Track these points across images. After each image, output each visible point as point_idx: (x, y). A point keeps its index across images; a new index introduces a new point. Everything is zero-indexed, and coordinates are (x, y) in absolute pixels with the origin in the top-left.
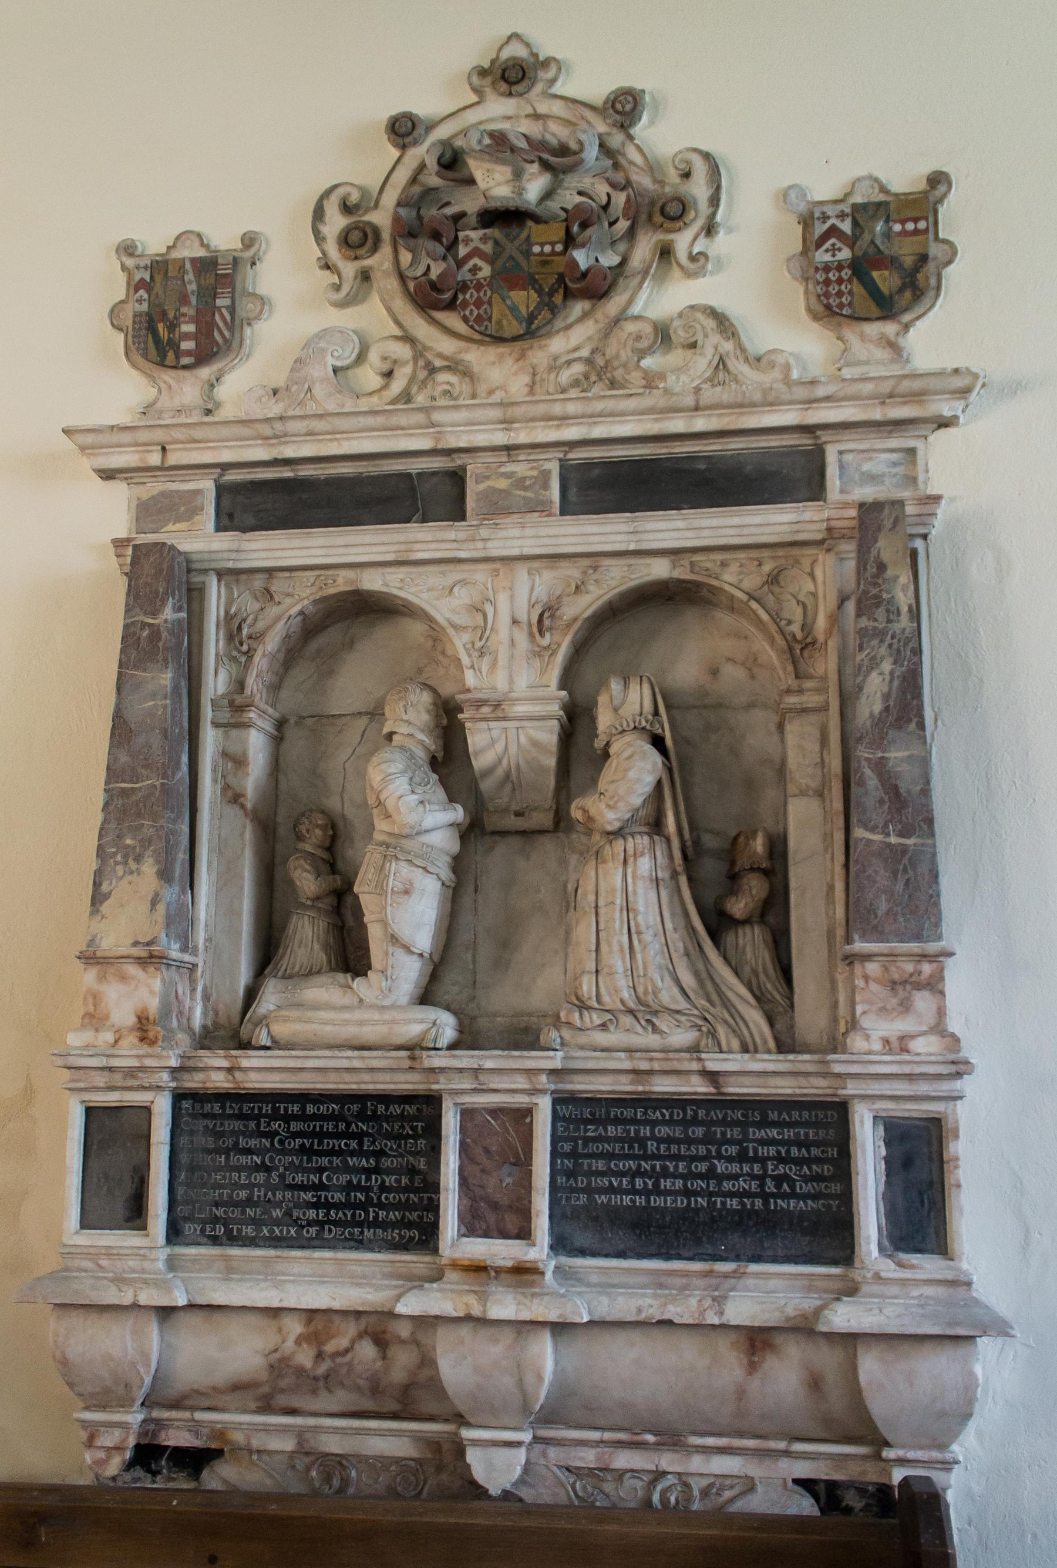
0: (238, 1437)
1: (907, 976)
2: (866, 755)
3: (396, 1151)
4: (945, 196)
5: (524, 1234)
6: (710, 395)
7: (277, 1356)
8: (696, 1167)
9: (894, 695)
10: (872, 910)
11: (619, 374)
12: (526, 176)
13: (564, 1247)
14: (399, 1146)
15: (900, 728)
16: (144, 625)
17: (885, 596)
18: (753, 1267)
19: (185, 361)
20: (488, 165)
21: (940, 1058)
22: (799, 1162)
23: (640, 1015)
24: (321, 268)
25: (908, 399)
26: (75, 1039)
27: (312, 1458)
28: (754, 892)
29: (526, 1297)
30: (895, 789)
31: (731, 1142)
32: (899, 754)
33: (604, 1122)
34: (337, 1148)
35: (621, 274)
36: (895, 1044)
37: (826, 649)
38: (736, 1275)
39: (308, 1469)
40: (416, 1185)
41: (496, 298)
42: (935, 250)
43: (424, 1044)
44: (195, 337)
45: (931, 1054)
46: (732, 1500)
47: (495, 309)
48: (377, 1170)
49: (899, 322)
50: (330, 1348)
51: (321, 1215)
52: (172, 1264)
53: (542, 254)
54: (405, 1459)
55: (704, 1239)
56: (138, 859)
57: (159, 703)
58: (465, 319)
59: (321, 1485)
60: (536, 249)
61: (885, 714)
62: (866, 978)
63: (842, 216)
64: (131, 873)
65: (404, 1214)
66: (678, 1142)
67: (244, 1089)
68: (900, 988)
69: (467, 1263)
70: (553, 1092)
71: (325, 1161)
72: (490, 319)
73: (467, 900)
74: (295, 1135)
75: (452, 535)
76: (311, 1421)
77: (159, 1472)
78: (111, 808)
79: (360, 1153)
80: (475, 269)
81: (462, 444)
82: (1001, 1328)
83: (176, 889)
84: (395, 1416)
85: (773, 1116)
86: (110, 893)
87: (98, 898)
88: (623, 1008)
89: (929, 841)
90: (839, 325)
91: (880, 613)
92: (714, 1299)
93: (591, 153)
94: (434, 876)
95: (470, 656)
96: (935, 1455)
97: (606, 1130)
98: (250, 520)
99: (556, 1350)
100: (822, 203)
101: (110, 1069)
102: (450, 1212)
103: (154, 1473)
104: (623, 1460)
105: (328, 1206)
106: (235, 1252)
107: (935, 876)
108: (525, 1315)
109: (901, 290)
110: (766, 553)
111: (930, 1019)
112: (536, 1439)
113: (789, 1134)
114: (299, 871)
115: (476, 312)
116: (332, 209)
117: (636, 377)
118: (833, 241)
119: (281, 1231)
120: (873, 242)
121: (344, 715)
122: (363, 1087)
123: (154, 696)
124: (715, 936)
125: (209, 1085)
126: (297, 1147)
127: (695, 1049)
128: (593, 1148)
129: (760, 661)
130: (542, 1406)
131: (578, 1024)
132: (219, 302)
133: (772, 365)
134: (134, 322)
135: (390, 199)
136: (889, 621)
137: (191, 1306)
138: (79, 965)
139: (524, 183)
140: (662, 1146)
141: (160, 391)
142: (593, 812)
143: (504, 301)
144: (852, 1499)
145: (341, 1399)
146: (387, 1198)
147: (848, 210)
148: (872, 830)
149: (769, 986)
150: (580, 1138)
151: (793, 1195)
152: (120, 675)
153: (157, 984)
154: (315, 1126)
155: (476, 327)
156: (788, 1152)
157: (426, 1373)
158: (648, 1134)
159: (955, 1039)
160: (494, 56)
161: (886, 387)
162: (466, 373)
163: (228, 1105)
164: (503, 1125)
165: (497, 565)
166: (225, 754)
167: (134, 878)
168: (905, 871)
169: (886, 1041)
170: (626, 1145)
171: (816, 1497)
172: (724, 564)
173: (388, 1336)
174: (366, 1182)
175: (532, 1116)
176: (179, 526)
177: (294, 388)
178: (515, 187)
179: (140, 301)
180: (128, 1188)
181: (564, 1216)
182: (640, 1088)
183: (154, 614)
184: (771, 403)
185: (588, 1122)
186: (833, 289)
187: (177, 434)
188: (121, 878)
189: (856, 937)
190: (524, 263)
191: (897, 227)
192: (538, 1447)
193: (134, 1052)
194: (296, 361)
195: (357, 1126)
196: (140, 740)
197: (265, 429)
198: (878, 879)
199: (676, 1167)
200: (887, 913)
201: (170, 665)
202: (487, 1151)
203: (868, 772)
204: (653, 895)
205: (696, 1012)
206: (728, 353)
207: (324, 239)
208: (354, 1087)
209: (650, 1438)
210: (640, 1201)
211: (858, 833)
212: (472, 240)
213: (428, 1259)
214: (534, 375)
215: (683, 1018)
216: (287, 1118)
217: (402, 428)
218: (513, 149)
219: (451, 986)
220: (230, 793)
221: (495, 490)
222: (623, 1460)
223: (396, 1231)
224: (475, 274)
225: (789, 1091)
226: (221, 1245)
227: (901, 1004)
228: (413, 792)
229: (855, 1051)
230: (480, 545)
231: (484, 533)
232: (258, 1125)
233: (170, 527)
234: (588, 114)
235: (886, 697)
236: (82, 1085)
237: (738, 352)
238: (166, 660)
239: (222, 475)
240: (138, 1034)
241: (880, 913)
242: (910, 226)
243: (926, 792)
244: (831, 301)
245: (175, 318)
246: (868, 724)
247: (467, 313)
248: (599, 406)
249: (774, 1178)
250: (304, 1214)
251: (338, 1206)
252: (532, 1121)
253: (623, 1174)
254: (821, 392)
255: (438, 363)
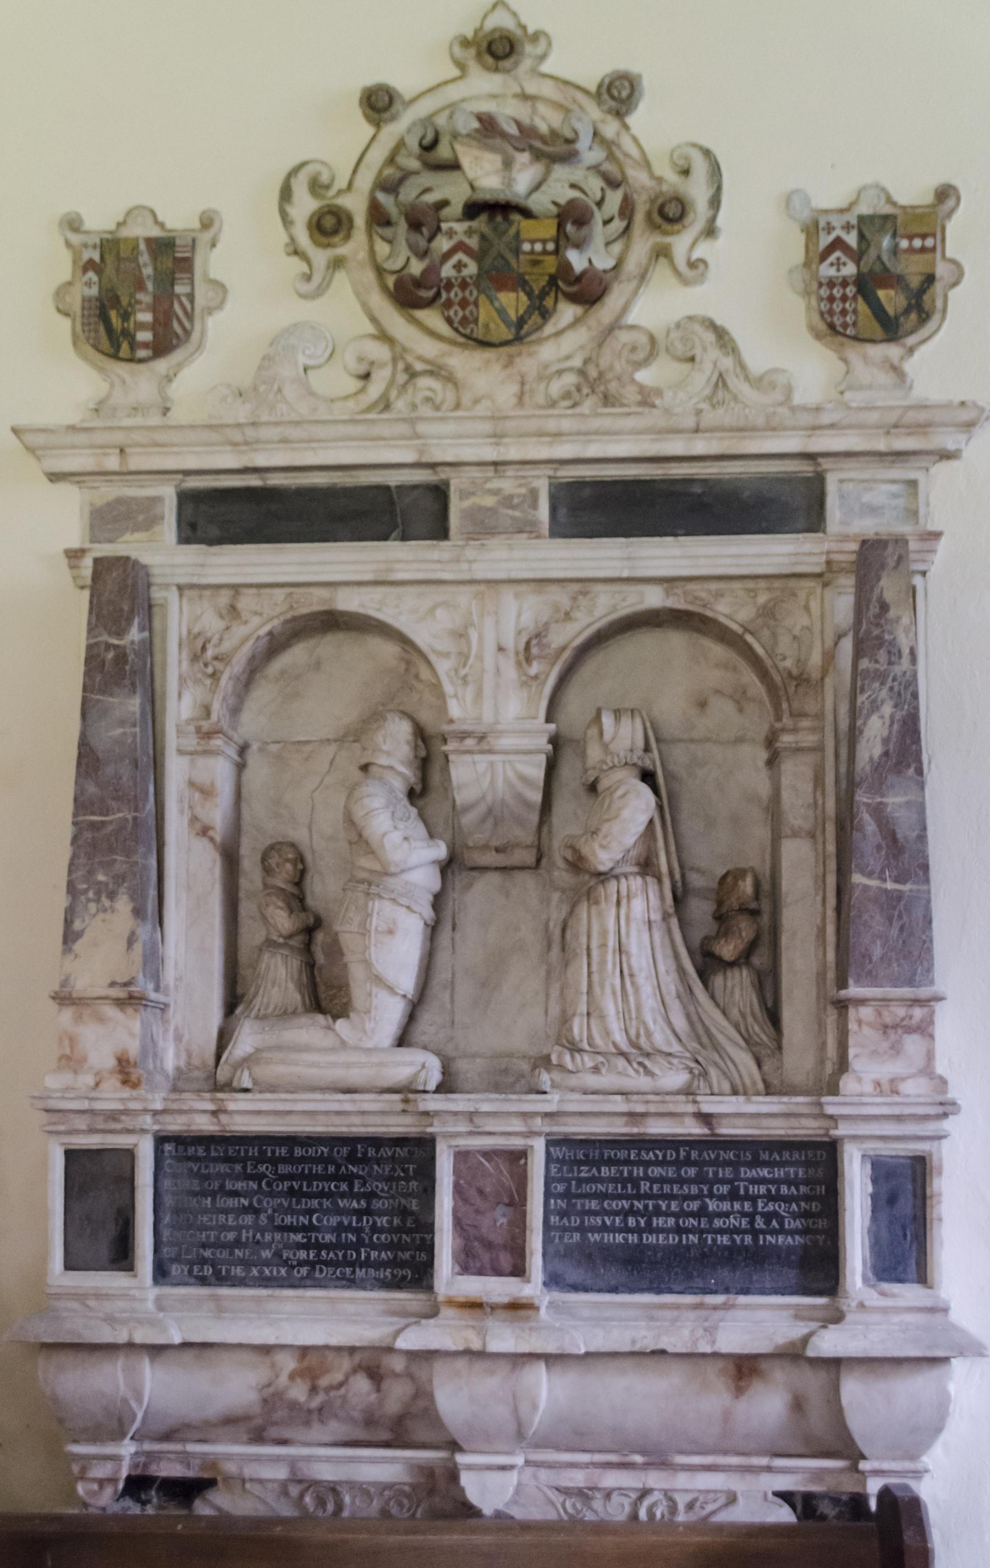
0: (231, 1468)
1: (898, 1020)
2: (865, 800)
3: (388, 1192)
4: (953, 211)
5: (519, 1271)
6: (711, 417)
7: (271, 1390)
8: (688, 1206)
9: (894, 739)
10: (867, 956)
11: (613, 387)
12: (517, 166)
13: (557, 1283)
14: (390, 1188)
15: (899, 772)
16: (108, 646)
17: (887, 637)
18: (742, 1299)
19: (142, 353)
20: (476, 152)
21: (929, 1100)
22: (788, 1200)
23: (632, 1057)
24: (289, 254)
25: (911, 430)
26: (54, 1082)
27: (306, 1485)
28: (744, 934)
29: (523, 1331)
30: (894, 839)
31: (723, 1181)
32: (900, 799)
33: (598, 1163)
34: (326, 1190)
35: (616, 278)
36: (886, 1087)
37: (823, 686)
38: (726, 1307)
39: (302, 1496)
40: (408, 1225)
41: (483, 299)
42: (941, 270)
43: (413, 1087)
44: (153, 327)
45: (919, 1096)
46: (714, 1513)
47: (482, 310)
48: (368, 1212)
49: (904, 346)
50: (324, 1382)
51: (312, 1255)
52: (160, 1305)
53: (532, 252)
54: (400, 1484)
55: (695, 1274)
56: (112, 896)
57: (128, 730)
58: (449, 321)
59: (315, 1510)
60: (526, 247)
61: (884, 759)
62: (860, 1022)
63: (847, 227)
64: (105, 910)
65: (396, 1254)
66: (671, 1181)
67: (231, 1132)
68: (890, 1031)
69: (463, 1300)
70: (547, 1134)
71: (315, 1203)
72: (476, 321)
73: (445, 937)
74: (283, 1178)
75: (436, 555)
76: (305, 1451)
77: (149, 1501)
78: (80, 842)
79: (351, 1195)
80: (459, 266)
81: (449, 458)
82: (972, 1349)
83: (149, 927)
84: (387, 1445)
85: (765, 1156)
86: (83, 931)
87: (70, 937)
88: (614, 1051)
89: (924, 887)
90: (842, 345)
91: (882, 655)
92: (705, 1330)
93: (583, 143)
94: (418, 916)
95: (453, 683)
96: (908, 1465)
97: (599, 1172)
98: (214, 531)
99: (549, 1380)
100: (826, 212)
101: (92, 1112)
102: (445, 1250)
103: (144, 1503)
104: (611, 1479)
105: (319, 1246)
106: (224, 1291)
107: (928, 921)
108: (524, 1348)
109: (907, 311)
110: (762, 584)
111: (920, 1062)
112: (528, 1463)
113: (779, 1173)
114: (271, 908)
115: (461, 314)
116: (300, 188)
117: (631, 394)
118: (838, 254)
119: (271, 1272)
120: (879, 258)
121: (333, 760)
122: (354, 1129)
123: (122, 723)
124: (704, 976)
125: (194, 1128)
126: (285, 1189)
127: (688, 1092)
128: (586, 1188)
129: (749, 694)
130: (534, 1433)
131: (570, 1066)
132: (179, 289)
133: (773, 385)
134: (83, 308)
135: (365, 181)
136: (890, 663)
137: (186, 1345)
138: (53, 1006)
139: (514, 173)
140: (655, 1186)
141: (112, 385)
142: (585, 851)
143: (492, 302)
144: (826, 1508)
145: (335, 1429)
146: (378, 1239)
147: (854, 222)
148: (870, 875)
149: (757, 1028)
150: (573, 1179)
151: (782, 1231)
152: (85, 702)
153: (137, 1026)
154: (303, 1169)
155: (461, 329)
156: (778, 1190)
157: (421, 1403)
158: (641, 1174)
159: (943, 1082)
160: (478, 25)
161: (892, 417)
162: (450, 379)
163: (212, 1148)
164: (497, 1167)
165: (482, 588)
166: (192, 784)
167: (108, 916)
168: (900, 917)
169: (878, 1084)
170: (619, 1186)
171: (793, 1507)
172: (719, 595)
173: (382, 1371)
174: (357, 1223)
175: (526, 1158)
176: (138, 536)
177: (262, 388)
178: (504, 178)
179: (89, 284)
180: (111, 1230)
181: (557, 1253)
182: (635, 1130)
183: (120, 634)
184: (773, 428)
185: (580, 1163)
186: (837, 306)
187: (137, 437)
188: (94, 916)
189: (851, 982)
190: (513, 261)
191: (904, 244)
192: (529, 1471)
193: (119, 1095)
194: (264, 359)
195: (347, 1168)
196: (110, 770)
197: (237, 436)
198: (874, 924)
199: (669, 1206)
200: (882, 958)
201: (139, 689)
202: (481, 1192)
203: (866, 817)
204: (646, 936)
205: (688, 1055)
206: (727, 371)
207: (292, 223)
208: (344, 1129)
209: (638, 1459)
210: (633, 1239)
211: (857, 878)
212: (456, 233)
213: (422, 1296)
214: (523, 384)
215: (675, 1061)
216: (275, 1161)
217: (384, 439)
218: (504, 135)
219: (427, 1026)
220: (198, 826)
221: (480, 508)
222: (611, 1479)
223: (389, 1270)
224: (459, 271)
225: (782, 1132)
226: (210, 1285)
227: (892, 1047)
228: (395, 828)
229: (847, 1093)
230: (465, 566)
231: (470, 553)
232: (245, 1168)
233: (128, 537)
234: (580, 96)
235: (886, 741)
236: (62, 1128)
237: (738, 370)
238: (133, 685)
239: (182, 481)
240: (120, 1077)
241: (874, 959)
242: (917, 243)
243: (922, 837)
244: (835, 319)
245: (130, 304)
246: (868, 768)
247: (452, 313)
248: (596, 423)
249: (763, 1215)
250: (295, 1255)
251: (329, 1247)
252: (526, 1164)
253: (617, 1213)
254: (825, 419)
255: (419, 366)
